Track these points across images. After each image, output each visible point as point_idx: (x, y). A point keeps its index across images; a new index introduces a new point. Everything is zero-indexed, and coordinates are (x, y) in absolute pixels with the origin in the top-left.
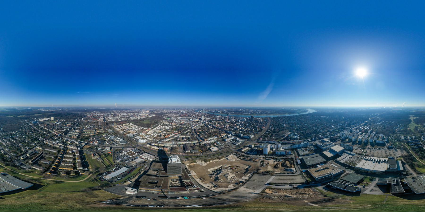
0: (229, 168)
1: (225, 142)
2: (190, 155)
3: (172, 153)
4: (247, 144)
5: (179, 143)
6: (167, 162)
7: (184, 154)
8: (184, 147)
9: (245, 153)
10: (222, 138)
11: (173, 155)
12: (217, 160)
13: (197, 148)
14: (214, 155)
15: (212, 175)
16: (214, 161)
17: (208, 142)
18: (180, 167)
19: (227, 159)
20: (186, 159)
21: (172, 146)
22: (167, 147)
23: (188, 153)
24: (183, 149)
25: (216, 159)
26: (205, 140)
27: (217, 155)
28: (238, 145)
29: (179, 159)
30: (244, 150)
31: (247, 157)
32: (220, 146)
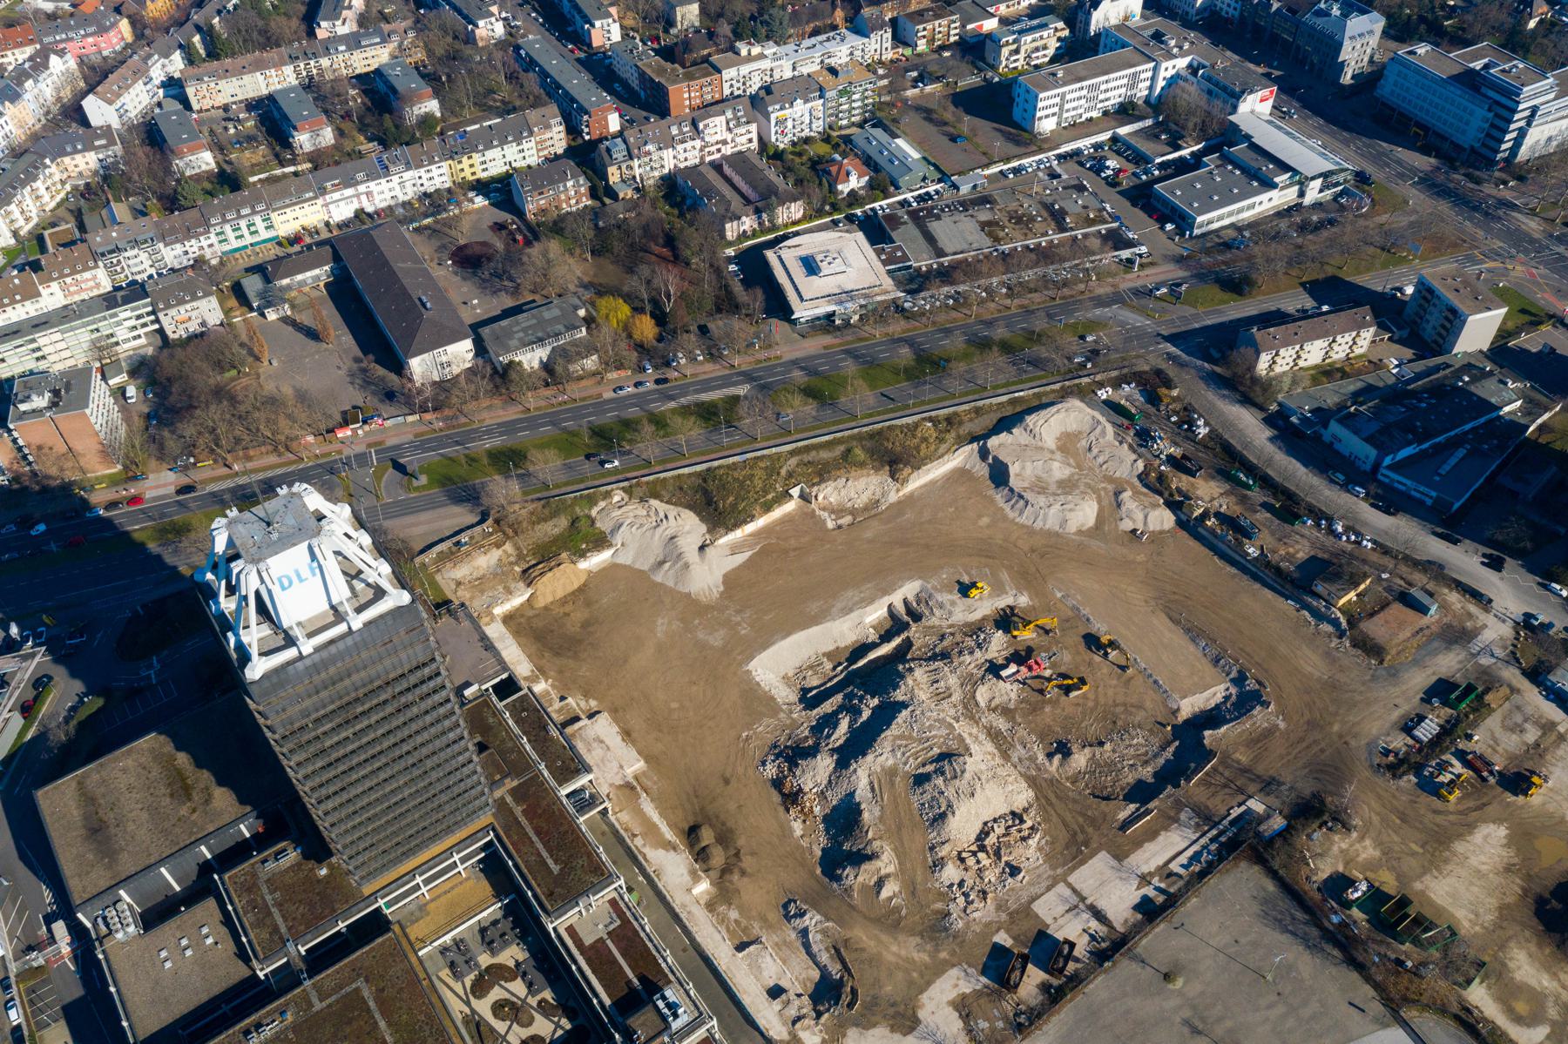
0: (998, 644)
1: (1022, 135)
2: (492, 413)
3: (209, 475)
4: (1390, 248)
5: (234, 236)
6: (224, 670)
7: (396, 427)
8: (342, 291)
9: (1279, 422)
10: (976, 49)
11: (246, 498)
12: (861, 488)
13: (568, 267)
14: (820, 389)
15: (795, 754)
16: (829, 493)
17: (726, 136)
18: (422, 676)
19: (999, 475)
20: (461, 515)
21: (129, 331)
22: (67, 391)
23: (444, 388)
24: (342, 339)
25: (847, 462)
26: (684, 95)
27: (860, 395)
28: (1224, 243)
29: (360, 546)
30: (1284, 361)
31: (1289, 507)
32: (923, 214)
